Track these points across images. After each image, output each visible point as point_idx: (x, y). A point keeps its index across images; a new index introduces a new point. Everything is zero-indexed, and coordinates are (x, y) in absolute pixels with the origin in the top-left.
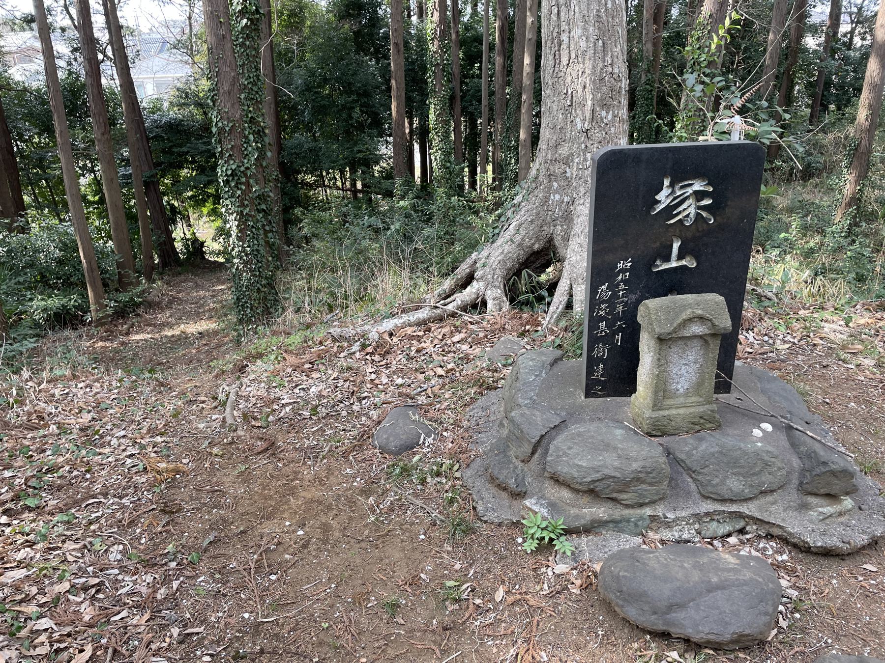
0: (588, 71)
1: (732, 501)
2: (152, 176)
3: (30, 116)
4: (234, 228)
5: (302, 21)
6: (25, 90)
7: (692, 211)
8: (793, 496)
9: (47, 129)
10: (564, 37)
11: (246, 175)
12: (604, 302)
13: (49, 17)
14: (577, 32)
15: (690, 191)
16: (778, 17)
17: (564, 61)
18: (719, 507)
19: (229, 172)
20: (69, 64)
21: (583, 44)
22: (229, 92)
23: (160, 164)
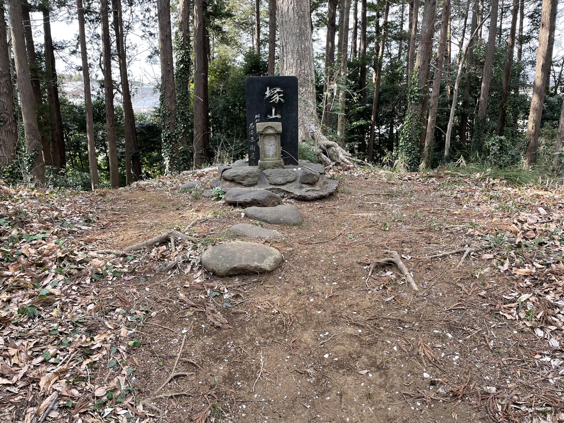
0: (294, 72)
1: (280, 185)
3: (74, 120)
4: (168, 164)
5: (228, 75)
6: (73, 106)
7: (278, 98)
8: (297, 184)
9: (82, 129)
10: (285, 58)
11: (175, 137)
12: (252, 130)
13: (90, 68)
14: (290, 56)
15: (276, 91)
16: (487, 74)
17: (285, 68)
18: (274, 187)
19: (167, 135)
20: (99, 93)
21: (292, 61)
22: (170, 97)
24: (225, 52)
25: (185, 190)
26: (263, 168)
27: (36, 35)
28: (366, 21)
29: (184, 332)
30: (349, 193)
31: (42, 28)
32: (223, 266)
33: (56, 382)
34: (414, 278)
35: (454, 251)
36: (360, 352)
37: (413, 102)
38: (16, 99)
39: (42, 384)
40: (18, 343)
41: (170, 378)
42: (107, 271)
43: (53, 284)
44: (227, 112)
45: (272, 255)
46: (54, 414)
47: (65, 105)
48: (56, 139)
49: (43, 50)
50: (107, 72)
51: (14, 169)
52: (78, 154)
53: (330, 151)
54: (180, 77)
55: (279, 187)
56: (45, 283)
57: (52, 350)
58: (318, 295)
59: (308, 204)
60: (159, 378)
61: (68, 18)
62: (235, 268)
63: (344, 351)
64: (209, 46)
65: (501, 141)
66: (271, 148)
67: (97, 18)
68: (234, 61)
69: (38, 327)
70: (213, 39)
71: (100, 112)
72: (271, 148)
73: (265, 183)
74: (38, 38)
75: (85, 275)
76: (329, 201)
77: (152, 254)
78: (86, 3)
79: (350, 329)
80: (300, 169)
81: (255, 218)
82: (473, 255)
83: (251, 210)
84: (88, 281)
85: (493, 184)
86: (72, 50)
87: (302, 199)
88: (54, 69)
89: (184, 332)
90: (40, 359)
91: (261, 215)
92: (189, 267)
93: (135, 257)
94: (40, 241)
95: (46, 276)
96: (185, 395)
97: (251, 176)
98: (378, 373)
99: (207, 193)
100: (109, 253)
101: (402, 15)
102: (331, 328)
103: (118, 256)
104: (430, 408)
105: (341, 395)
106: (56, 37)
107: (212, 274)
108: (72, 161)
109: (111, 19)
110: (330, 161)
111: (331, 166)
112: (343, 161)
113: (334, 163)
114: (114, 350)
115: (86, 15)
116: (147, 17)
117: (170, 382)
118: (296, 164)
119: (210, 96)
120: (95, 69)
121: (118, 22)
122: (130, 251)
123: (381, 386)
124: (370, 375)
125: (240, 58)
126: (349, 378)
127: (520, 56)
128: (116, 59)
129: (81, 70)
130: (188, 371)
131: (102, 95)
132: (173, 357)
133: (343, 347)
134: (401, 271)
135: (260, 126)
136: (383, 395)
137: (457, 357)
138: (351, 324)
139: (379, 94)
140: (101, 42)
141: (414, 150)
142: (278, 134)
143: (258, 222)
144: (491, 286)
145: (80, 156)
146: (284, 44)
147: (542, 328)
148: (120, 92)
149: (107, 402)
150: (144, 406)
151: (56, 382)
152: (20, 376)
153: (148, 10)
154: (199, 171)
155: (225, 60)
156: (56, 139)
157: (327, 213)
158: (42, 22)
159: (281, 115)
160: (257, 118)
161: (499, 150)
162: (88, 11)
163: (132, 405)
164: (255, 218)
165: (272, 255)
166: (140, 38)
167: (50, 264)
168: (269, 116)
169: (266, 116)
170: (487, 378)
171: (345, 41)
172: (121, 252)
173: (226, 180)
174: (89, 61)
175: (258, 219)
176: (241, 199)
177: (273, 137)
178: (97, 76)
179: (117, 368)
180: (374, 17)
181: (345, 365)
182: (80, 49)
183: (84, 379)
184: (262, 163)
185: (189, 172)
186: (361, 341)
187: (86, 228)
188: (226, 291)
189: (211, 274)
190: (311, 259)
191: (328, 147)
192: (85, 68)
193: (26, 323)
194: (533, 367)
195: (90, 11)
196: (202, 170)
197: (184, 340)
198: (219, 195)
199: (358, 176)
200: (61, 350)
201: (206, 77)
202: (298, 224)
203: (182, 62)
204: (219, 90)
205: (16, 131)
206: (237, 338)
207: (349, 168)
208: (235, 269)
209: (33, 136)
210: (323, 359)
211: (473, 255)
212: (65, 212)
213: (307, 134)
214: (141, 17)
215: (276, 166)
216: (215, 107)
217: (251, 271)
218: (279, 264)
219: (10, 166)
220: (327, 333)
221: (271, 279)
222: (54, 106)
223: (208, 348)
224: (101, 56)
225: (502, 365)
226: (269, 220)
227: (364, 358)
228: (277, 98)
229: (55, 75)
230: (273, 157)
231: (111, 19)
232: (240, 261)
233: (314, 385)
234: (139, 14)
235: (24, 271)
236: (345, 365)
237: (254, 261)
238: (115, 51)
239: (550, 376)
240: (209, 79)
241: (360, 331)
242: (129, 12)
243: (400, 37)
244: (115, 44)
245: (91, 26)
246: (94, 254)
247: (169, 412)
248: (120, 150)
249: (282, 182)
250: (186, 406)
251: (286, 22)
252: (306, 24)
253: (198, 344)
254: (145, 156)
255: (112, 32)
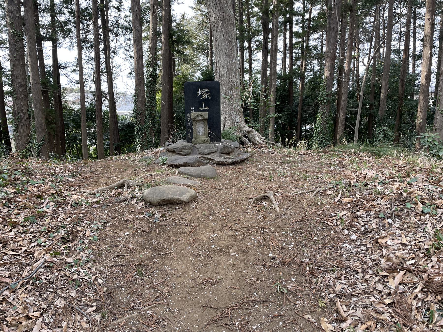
2: (118, 145)
3: (73, 120)
7: (206, 96)
8: (218, 154)
10: (218, 71)
14: (221, 69)
17: (218, 77)
18: (202, 156)
20: (92, 100)
21: (223, 72)
22: (141, 101)
23: (122, 141)
24: (187, 69)
25: (142, 160)
26: (196, 143)
27: (47, 58)
28: (292, 47)
29: (126, 234)
30: (256, 161)
31: (51, 53)
32: (156, 198)
33: (44, 255)
34: (279, 205)
35: (310, 191)
36: (234, 244)
37: (322, 103)
38: (30, 102)
39: (36, 255)
40: (23, 236)
41: (113, 256)
42: (82, 202)
43: (47, 206)
44: (178, 109)
45: (189, 192)
46: (41, 270)
47: (67, 109)
48: (59, 134)
49: (52, 69)
50: (98, 83)
51: (27, 153)
52: (75, 145)
53: (250, 136)
54: (149, 87)
55: (206, 156)
56: (41, 206)
57: (43, 239)
58: (216, 216)
59: (225, 167)
60: (107, 256)
61: (70, 46)
62: (164, 200)
63: (224, 243)
64: (174, 65)
65: (384, 130)
66: (201, 129)
67: (92, 46)
68: (194, 76)
69: (35, 228)
70: (178, 60)
71: (91, 114)
72: (201, 130)
73: (196, 153)
74: (48, 60)
75: (68, 204)
76: (240, 165)
77: (112, 193)
78: (84, 35)
79: (231, 232)
80: (221, 144)
81: (184, 174)
82: (321, 193)
83: (181, 169)
84: (69, 207)
85: (361, 156)
86: (73, 69)
87: (221, 164)
88: (59, 82)
89: (126, 234)
90: (36, 244)
91: (188, 171)
92: (135, 200)
93: (101, 195)
94: (40, 184)
95: (43, 203)
96: (122, 265)
97: (186, 148)
98: (242, 254)
99: (156, 162)
100: (85, 193)
101: (322, 40)
102: (220, 232)
103: (90, 194)
104: (268, 270)
105: (217, 266)
106: (61, 59)
107: (149, 204)
108: (70, 151)
109: (102, 46)
110: (248, 141)
111: (249, 145)
112: (258, 142)
113: (251, 143)
114: (81, 241)
115: (84, 43)
116: (128, 45)
117: (113, 258)
118: (220, 141)
119: (174, 102)
120: (89, 83)
121: (107, 48)
122: (98, 191)
123: (242, 261)
124: (237, 255)
125: (198, 74)
126: (224, 257)
127: (414, 70)
128: (105, 75)
129: (79, 83)
130: (125, 253)
131: (94, 102)
132: (117, 246)
133: (224, 242)
134: (271, 202)
135: (193, 115)
136: (242, 264)
137: (292, 245)
138: (232, 230)
139: (304, 100)
140: (93, 63)
141: (325, 139)
142: (205, 120)
143: (185, 176)
144: (326, 209)
145: (76, 147)
146: (217, 61)
147: (348, 229)
148: (107, 99)
149: (74, 265)
150: (96, 269)
151: (44, 255)
152: (23, 251)
153: (129, 40)
154: (156, 150)
155: (186, 75)
156: (59, 134)
157: (236, 172)
158: (51, 48)
159: (209, 107)
160: (192, 110)
161: (383, 137)
162: (86, 40)
163: (89, 268)
164: (184, 174)
165: (189, 192)
166: (123, 60)
167: (46, 197)
168: (200, 108)
169: (198, 109)
170: (307, 255)
171: (274, 60)
172: (92, 192)
173: (169, 151)
174: (85, 77)
175: (186, 174)
176: (177, 163)
177: (202, 122)
178: (90, 88)
179: (82, 250)
180: (299, 42)
181: (223, 251)
182: (78, 69)
183: (61, 254)
184: (194, 140)
185: (148, 150)
186: (236, 239)
187: (71, 179)
188: (157, 213)
189: (149, 204)
190: (216, 196)
191: (249, 132)
192: (82, 82)
193: (29, 226)
194: (336, 249)
195: (87, 41)
196: (158, 149)
197: (125, 238)
198: (164, 161)
199: (268, 152)
200: (49, 240)
201: (171, 87)
202: (213, 178)
203: (150, 76)
204: (181, 98)
205: (29, 125)
206: (159, 238)
207: (262, 147)
208: (164, 200)
209: (42, 130)
210: (211, 248)
211: (321, 193)
212: (58, 171)
213: (233, 124)
214: (124, 45)
215: (204, 142)
216: (178, 110)
217: (174, 202)
218: (194, 199)
219: (24, 151)
220: (216, 235)
221: (187, 207)
222: (58, 109)
223: (140, 243)
224: (94, 73)
225: (318, 248)
226: (193, 175)
227: (236, 247)
228: (206, 96)
229: (59, 87)
230: (202, 136)
231: (102, 46)
232: (167, 195)
233: (201, 261)
234: (122, 42)
235: (29, 199)
236: (223, 251)
237: (177, 195)
238: (104, 70)
239: (345, 253)
240: (173, 89)
241: (237, 233)
242: (115, 41)
243: (320, 57)
244: (104, 65)
245: (87, 52)
246: (75, 193)
247: (111, 273)
248: (106, 143)
249: (208, 152)
250: (122, 270)
251: (219, 45)
252: (233, 47)
253: (134, 241)
254: (125, 147)
255: (102, 56)
